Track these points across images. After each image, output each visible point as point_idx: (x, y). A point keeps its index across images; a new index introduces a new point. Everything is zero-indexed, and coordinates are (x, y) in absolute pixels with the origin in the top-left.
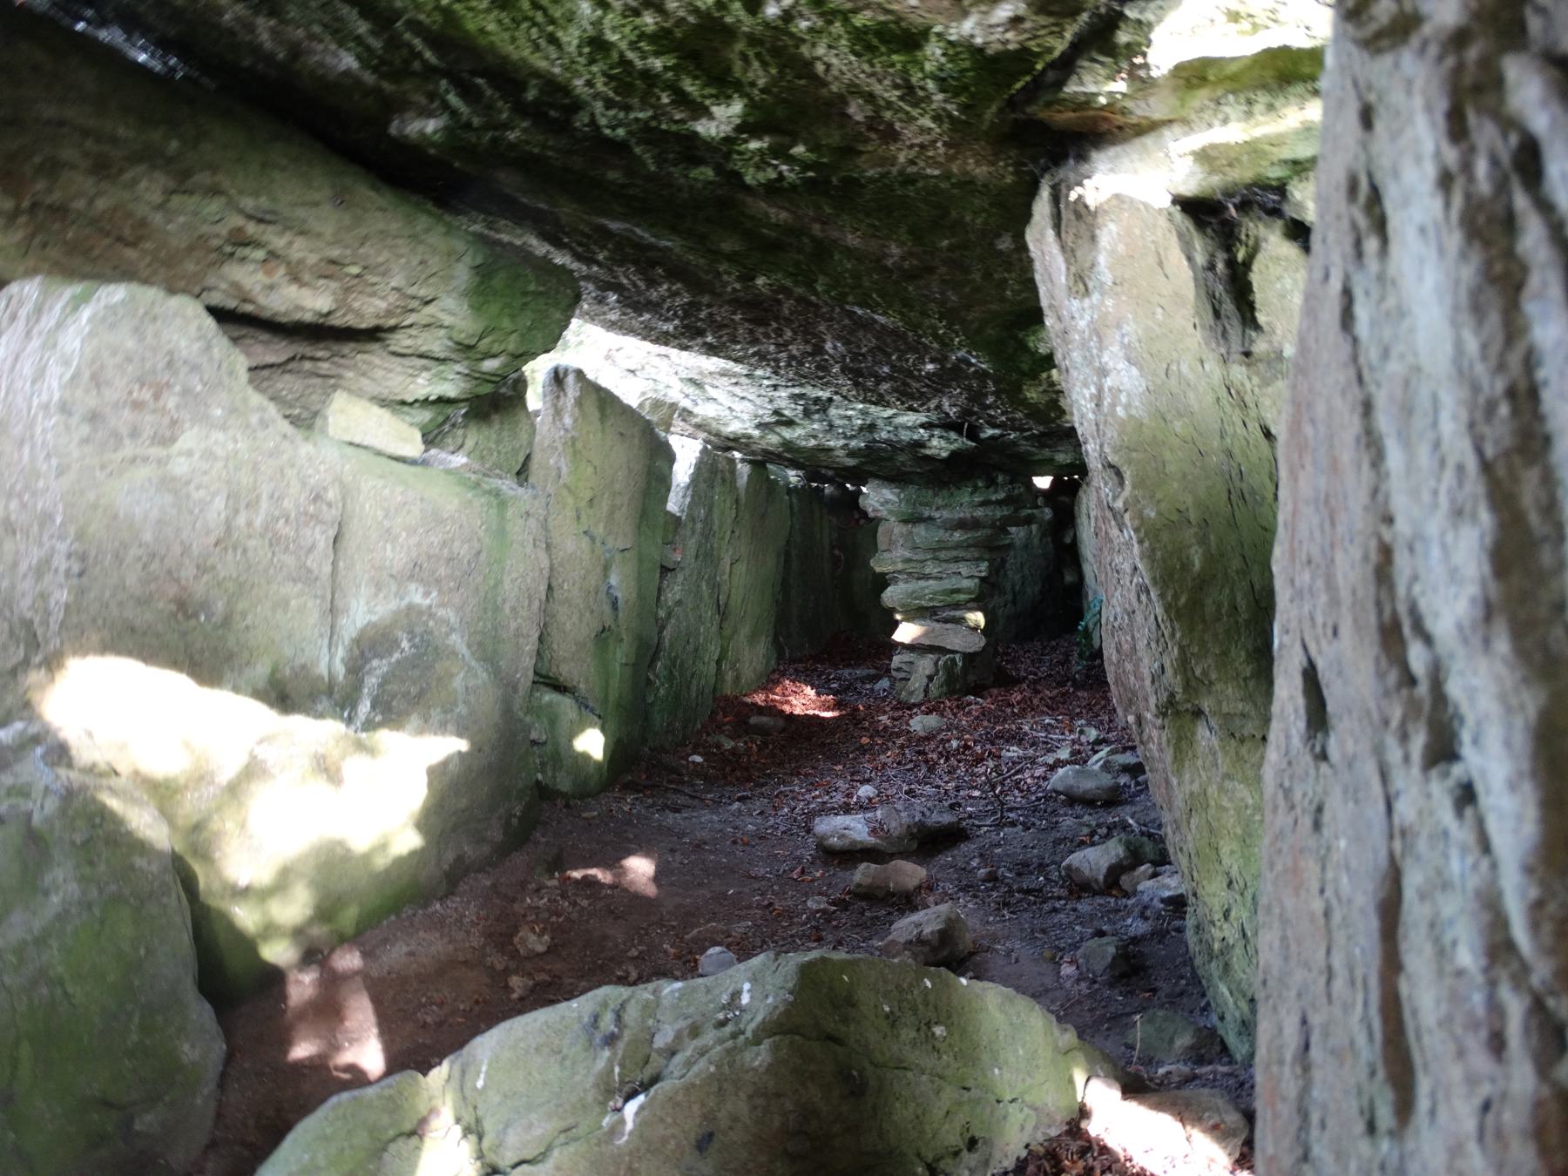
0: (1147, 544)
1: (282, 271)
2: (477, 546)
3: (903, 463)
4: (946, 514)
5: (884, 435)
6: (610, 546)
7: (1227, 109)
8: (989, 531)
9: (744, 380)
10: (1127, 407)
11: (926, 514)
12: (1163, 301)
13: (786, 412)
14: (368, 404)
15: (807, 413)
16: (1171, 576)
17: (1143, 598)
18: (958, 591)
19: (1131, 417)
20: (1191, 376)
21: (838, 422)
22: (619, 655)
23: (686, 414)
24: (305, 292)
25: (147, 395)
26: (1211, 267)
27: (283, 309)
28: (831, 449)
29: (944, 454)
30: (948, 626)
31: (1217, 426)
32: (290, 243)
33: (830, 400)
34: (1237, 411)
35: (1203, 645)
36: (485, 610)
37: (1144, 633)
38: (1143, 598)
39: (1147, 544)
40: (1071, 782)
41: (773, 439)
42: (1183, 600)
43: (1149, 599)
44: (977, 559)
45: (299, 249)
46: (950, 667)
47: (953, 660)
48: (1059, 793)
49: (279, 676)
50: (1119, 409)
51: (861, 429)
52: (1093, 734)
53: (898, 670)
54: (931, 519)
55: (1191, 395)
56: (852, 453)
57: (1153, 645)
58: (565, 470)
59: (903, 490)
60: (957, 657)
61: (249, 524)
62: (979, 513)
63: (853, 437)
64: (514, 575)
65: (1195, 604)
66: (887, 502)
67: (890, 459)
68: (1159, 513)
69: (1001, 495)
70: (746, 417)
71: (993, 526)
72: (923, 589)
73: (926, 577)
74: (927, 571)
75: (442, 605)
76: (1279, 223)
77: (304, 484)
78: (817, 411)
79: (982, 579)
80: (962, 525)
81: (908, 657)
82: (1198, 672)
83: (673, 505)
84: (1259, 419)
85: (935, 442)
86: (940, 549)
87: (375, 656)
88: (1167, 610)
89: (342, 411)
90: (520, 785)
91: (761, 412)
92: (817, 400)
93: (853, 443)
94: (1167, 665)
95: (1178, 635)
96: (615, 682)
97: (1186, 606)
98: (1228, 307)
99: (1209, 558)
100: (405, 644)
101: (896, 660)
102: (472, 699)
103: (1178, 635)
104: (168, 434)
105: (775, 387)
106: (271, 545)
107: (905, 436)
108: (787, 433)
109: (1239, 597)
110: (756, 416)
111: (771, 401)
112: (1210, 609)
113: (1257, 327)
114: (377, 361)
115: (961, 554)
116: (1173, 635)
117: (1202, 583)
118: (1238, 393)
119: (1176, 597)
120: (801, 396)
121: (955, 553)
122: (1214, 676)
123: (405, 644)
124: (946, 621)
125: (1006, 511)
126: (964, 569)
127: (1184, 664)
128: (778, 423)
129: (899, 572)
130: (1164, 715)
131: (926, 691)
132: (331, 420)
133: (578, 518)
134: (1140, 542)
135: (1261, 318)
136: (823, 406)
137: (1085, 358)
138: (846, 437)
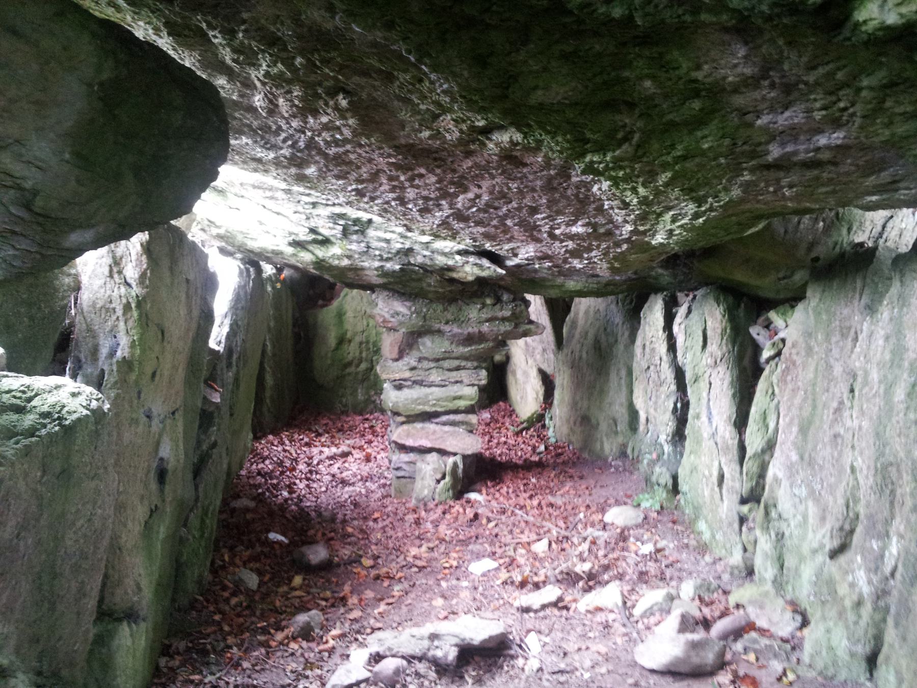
4: (456, 330)
5: (420, 259)
8: (491, 344)
9: (280, 195)
11: (437, 326)
13: (321, 230)
15: (345, 233)
18: (460, 398)
21: (375, 244)
22: (162, 529)
28: (363, 269)
29: (470, 278)
33: (370, 221)
41: (306, 257)
44: (475, 368)
51: (399, 252)
54: (439, 331)
60: (458, 459)
62: (486, 328)
67: (419, 280)
69: (507, 313)
72: (427, 395)
78: (356, 232)
83: (217, 338)
85: (468, 268)
86: (444, 359)
92: (357, 221)
93: (388, 265)
105: (314, 205)
107: (441, 261)
108: (321, 252)
110: (291, 234)
115: (463, 363)
120: (342, 216)
121: (456, 363)
126: (463, 375)
128: (315, 241)
129: (405, 380)
136: (362, 227)
138: (382, 259)
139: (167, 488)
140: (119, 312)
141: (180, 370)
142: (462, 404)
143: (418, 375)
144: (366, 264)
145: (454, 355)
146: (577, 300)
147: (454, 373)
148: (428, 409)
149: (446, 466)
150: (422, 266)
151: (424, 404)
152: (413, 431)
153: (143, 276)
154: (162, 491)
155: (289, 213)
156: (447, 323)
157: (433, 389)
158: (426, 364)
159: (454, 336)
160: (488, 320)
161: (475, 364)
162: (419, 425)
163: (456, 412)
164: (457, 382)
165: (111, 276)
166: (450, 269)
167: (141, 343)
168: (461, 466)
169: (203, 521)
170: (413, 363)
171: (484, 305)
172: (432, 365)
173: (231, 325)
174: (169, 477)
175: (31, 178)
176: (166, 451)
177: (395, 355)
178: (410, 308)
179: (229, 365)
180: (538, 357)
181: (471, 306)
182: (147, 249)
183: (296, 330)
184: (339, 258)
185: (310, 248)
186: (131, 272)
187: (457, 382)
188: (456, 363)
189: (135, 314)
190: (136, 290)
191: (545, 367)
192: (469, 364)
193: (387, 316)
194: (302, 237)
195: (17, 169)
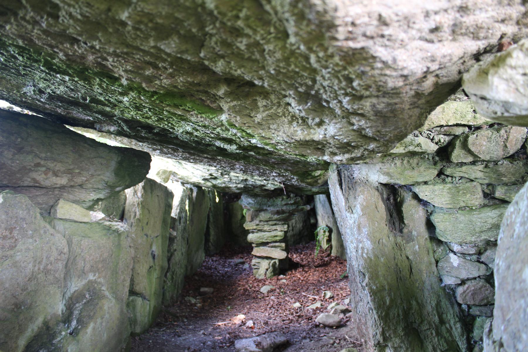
0: (373, 297)
1: (51, 173)
2: (111, 253)
3: (257, 192)
5: (251, 183)
6: (152, 237)
7: (396, 161)
8: (288, 214)
10: (367, 254)
11: (265, 208)
12: (377, 220)
13: (214, 175)
14: (71, 204)
16: (380, 306)
17: (371, 311)
18: (276, 236)
19: (368, 257)
20: (386, 243)
21: (233, 178)
23: (175, 174)
24: (58, 178)
25: (8, 233)
26: (388, 199)
27: (49, 185)
28: (230, 187)
29: (272, 189)
30: (273, 249)
31: (393, 256)
32: (56, 165)
34: (399, 251)
35: (389, 327)
36: (113, 275)
37: (370, 323)
38: (371, 311)
39: (373, 297)
40: (324, 320)
42: (384, 314)
43: (373, 312)
44: (283, 224)
45: (59, 167)
46: (274, 265)
47: (275, 262)
48: (320, 324)
49: (46, 320)
50: (364, 254)
51: (242, 180)
52: (329, 294)
53: (254, 265)
54: (266, 210)
55: (386, 249)
56: (238, 189)
57: (374, 326)
58: (138, 213)
59: (256, 199)
60: (277, 261)
61: (39, 269)
62: (284, 208)
63: (239, 183)
64: (123, 260)
65: (387, 315)
66: (250, 203)
67: (252, 190)
68: (377, 287)
69: (292, 202)
70: (199, 176)
71: (289, 212)
72: (263, 235)
73: (265, 231)
74: (265, 229)
75: (99, 277)
76: (411, 193)
77: (57, 249)
78: (226, 174)
79: (285, 232)
80: (278, 213)
81: (258, 260)
82: (387, 335)
83: (174, 213)
84: (405, 254)
85: (269, 185)
86: (270, 221)
87: (77, 303)
88: (379, 317)
89: (62, 208)
90: (125, 337)
91: (204, 175)
93: (239, 186)
94: (378, 333)
95: (382, 324)
96: (154, 286)
97: (384, 315)
98: (395, 215)
99: (391, 301)
100: (87, 296)
101: (254, 261)
102: (110, 311)
103: (382, 324)
104: (14, 245)
106: (46, 274)
108: (214, 182)
109: (400, 311)
110: (203, 176)
111: (208, 170)
112: (391, 315)
113: (403, 223)
114: (77, 190)
115: (277, 222)
116: (380, 324)
117: (389, 308)
118: (399, 245)
119: (382, 313)
121: (275, 222)
122: (392, 336)
123: (87, 296)
124: (272, 247)
125: (294, 207)
126: (278, 228)
127: (383, 333)
129: (255, 229)
130: (376, 346)
131: (265, 274)
132: (58, 211)
133: (143, 230)
134: (371, 296)
135: (406, 222)
137: (352, 233)
138: (236, 183)
139: (156, 261)
140: (136, 206)
141: (158, 222)
142: (278, 238)
143: (259, 228)
144: (231, 186)
145: (273, 219)
146: (318, 196)
147: (274, 227)
148: (264, 241)
149: (99, 200)
150: (252, 185)
151: (262, 239)
152: (259, 250)
153: (142, 195)
154: (154, 261)
155: (202, 169)
156: (269, 206)
157: (266, 233)
158: (262, 223)
159: (272, 211)
160: (285, 205)
161: (283, 222)
162: (261, 248)
163: (276, 242)
164: (275, 230)
165: (134, 195)
166: (264, 186)
167: (142, 214)
168: (278, 263)
169: (172, 277)
170: (257, 222)
171: (283, 199)
172: (266, 223)
173: (180, 209)
174: (156, 257)
175: (106, 179)
176: (154, 248)
177: (250, 219)
178: (254, 201)
179: (180, 223)
180: (326, 220)
181: (279, 199)
182: (144, 187)
183: (226, 211)
184: (221, 184)
185: (210, 180)
186: (139, 194)
187: (275, 230)
188: (275, 222)
189: (141, 206)
190: (141, 199)
191: (329, 225)
192: (280, 223)
193: (246, 205)
194: (207, 177)
195: (104, 178)
